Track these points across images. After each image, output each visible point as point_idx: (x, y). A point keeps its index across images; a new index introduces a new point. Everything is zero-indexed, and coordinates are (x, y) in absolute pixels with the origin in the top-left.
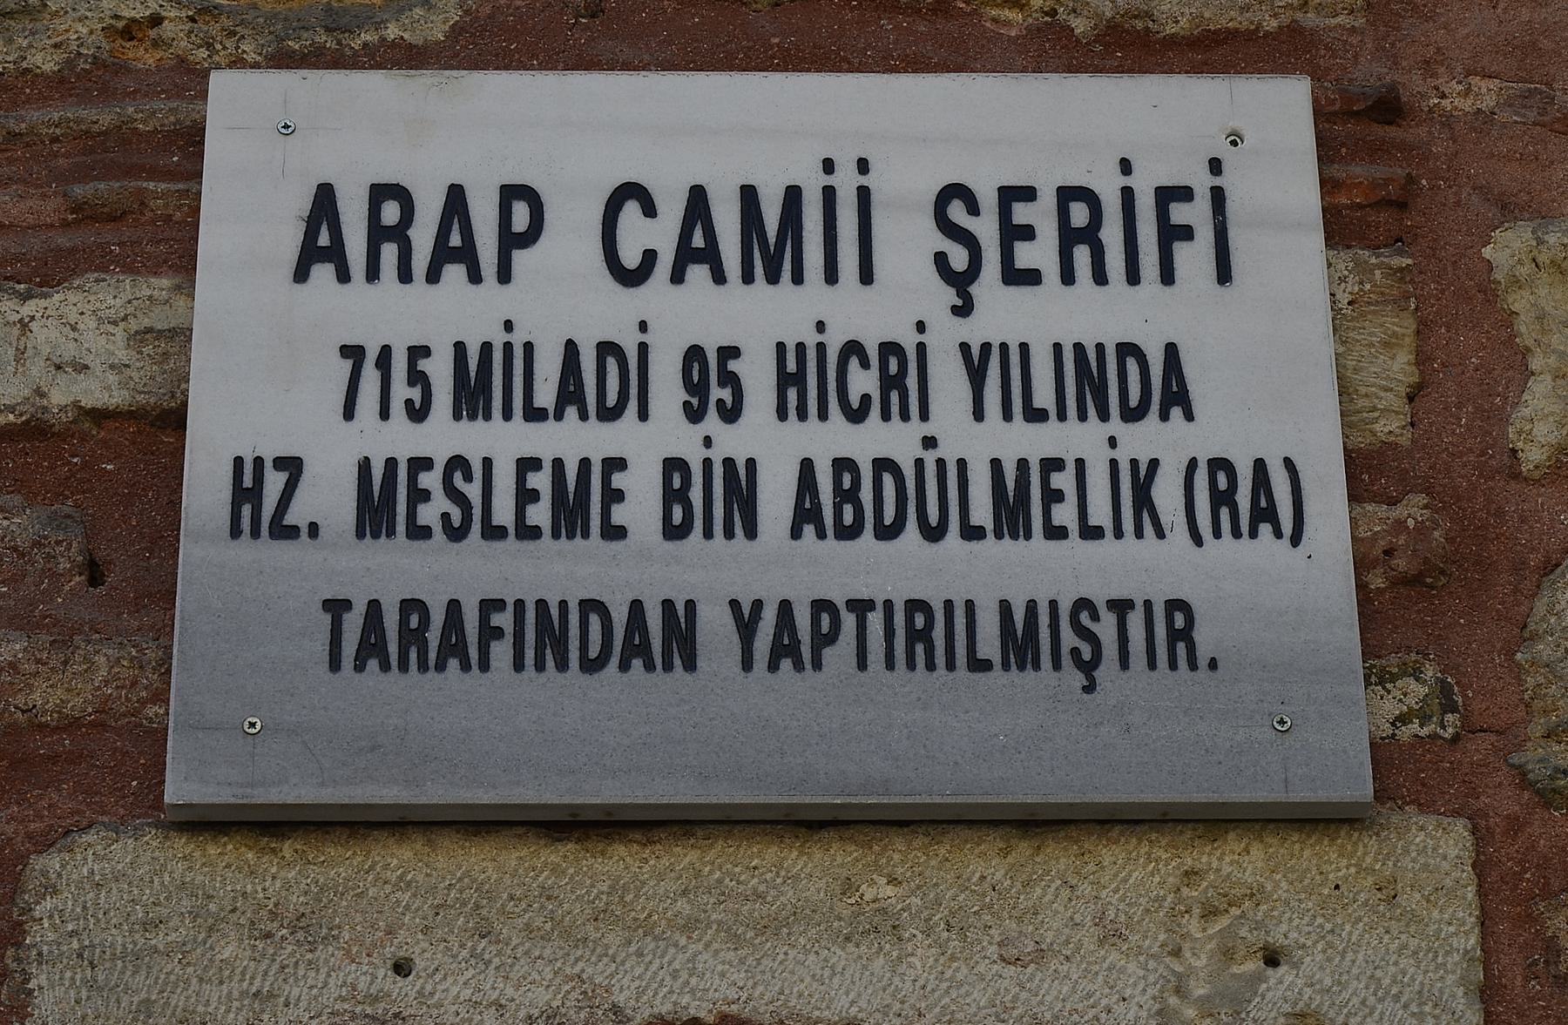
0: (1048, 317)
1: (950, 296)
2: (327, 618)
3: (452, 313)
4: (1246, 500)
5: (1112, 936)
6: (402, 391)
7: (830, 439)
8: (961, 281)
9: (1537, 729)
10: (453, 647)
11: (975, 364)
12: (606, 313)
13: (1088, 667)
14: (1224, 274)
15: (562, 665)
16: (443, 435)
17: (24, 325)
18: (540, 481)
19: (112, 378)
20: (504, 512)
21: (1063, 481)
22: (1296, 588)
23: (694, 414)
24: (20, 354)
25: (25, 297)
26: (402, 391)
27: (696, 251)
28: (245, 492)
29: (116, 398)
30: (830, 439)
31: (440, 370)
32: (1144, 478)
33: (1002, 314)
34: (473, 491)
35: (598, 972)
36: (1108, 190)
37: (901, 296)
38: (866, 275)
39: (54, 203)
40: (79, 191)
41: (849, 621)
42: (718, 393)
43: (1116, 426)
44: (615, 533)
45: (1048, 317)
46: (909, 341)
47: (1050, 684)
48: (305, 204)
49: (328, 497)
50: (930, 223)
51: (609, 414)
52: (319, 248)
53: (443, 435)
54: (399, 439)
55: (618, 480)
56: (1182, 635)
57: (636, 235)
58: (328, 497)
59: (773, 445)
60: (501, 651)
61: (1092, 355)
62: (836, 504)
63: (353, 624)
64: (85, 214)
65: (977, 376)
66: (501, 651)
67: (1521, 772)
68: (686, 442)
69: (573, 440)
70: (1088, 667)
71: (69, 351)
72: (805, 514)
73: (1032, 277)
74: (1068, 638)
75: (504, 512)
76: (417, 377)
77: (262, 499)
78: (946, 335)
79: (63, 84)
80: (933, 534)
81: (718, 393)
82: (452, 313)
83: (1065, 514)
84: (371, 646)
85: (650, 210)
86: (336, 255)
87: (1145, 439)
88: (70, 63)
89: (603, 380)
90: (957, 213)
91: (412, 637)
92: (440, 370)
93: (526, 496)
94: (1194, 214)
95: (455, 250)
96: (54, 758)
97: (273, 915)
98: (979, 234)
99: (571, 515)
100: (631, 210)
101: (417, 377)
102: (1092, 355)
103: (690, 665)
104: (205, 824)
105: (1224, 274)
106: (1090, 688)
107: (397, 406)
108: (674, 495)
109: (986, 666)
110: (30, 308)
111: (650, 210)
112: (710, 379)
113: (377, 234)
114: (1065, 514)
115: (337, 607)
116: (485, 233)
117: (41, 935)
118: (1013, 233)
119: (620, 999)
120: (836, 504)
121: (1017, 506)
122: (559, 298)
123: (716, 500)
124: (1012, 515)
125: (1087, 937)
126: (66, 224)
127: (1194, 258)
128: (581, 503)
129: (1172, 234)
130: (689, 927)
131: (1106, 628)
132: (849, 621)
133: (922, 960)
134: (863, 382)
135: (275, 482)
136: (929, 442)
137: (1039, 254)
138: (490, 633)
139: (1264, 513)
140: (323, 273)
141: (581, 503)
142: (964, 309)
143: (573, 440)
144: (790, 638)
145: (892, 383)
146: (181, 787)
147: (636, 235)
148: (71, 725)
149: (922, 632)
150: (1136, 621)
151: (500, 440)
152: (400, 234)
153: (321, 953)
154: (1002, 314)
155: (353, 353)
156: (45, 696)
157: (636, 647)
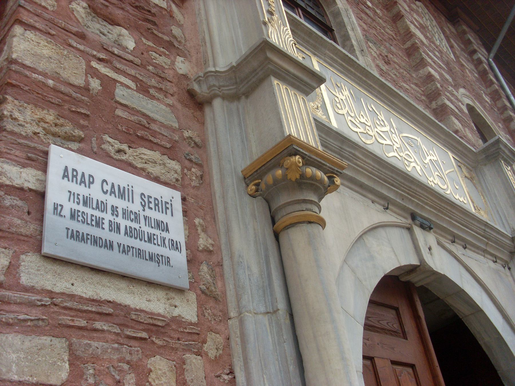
0: (155, 215)
1: (142, 208)
2: (66, 230)
3: (82, 190)
4: (175, 246)
5: (158, 300)
6: (76, 200)
7: (129, 223)
8: (144, 206)
9: (202, 283)
10: (83, 239)
11: (145, 218)
12: (102, 197)
13: (159, 263)
14: (172, 215)
15: (97, 245)
16: (81, 208)
17: (21, 173)
18: (94, 218)
19: (33, 184)
20: (89, 222)
21: (155, 237)
22: (180, 258)
23: (113, 214)
24: (20, 177)
25: (21, 168)
26: (76, 200)
27: (113, 192)
28: (55, 209)
29: (33, 188)
30: (129, 223)
31: (81, 198)
32: (164, 240)
33: (148, 213)
34: (85, 217)
35: (98, 291)
36: (160, 199)
37: (136, 207)
38: (133, 202)
39: (24, 155)
40: (29, 155)
41: (131, 249)
42: (115, 213)
43: (161, 232)
44: (103, 229)
45: (155, 215)
46: (138, 213)
47: (154, 264)
48: (64, 168)
49: (66, 212)
50: (140, 197)
51: (102, 211)
52: (65, 175)
53: (81, 208)
54: (75, 207)
55: (103, 221)
56: (169, 262)
57: (106, 187)
58: (66, 212)
59: (124, 223)
60: (89, 241)
61: (73, 211)
62: (130, 232)
63: (70, 232)
64: (29, 159)
65: (145, 220)
66: (89, 241)
67: (200, 288)
68: (112, 218)
69: (98, 214)
70: (159, 263)
71: (27, 179)
72: (126, 233)
73: (151, 209)
74: (156, 259)
75: (89, 222)
76: (78, 198)
77: (57, 209)
78: (142, 213)
79: (26, 137)
80: (141, 240)
81: (115, 213)
82: (82, 190)
83: (156, 242)
84: (72, 236)
85: (107, 184)
86: (67, 177)
87: (164, 234)
88: (27, 135)
89: (101, 206)
90: (143, 197)
91: (78, 236)
92: (81, 198)
93: (92, 220)
94: (169, 206)
95: (83, 182)
96: (24, 241)
97: (55, 273)
98: (146, 201)
99: (98, 225)
100: (105, 184)
101: (78, 198)
102: (73, 211)
103: (112, 250)
104: (48, 258)
105: (172, 215)
106: (159, 266)
107: (76, 202)
108: (110, 226)
109: (147, 260)
110: (22, 170)
111: (107, 184)
112: (114, 210)
113: (73, 176)
114: (156, 242)
115: (68, 229)
116: (87, 181)
117: (22, 268)
118: (150, 202)
119: (101, 296)
120: (130, 232)
121: (150, 239)
122: (95, 193)
123: (115, 228)
124: (150, 240)
125: (156, 299)
126: (26, 159)
127: (169, 212)
128: (99, 223)
129: (167, 208)
130: (109, 287)
131: (160, 258)
132: (131, 249)
133: (137, 299)
134: (133, 217)
135: (59, 208)
136: (140, 227)
137: (152, 205)
138: (88, 239)
139: (177, 248)
140: (66, 179)
141: (99, 223)
142: (144, 210)
143: (98, 214)
144: (125, 250)
145: (136, 218)
146: (46, 249)
147: (106, 187)
148: (27, 236)
149: (140, 253)
150: (164, 258)
151: (89, 211)
152: (76, 176)
153: (62, 280)
154: (148, 213)
155: (70, 192)
156: (23, 231)
157: (106, 246)
